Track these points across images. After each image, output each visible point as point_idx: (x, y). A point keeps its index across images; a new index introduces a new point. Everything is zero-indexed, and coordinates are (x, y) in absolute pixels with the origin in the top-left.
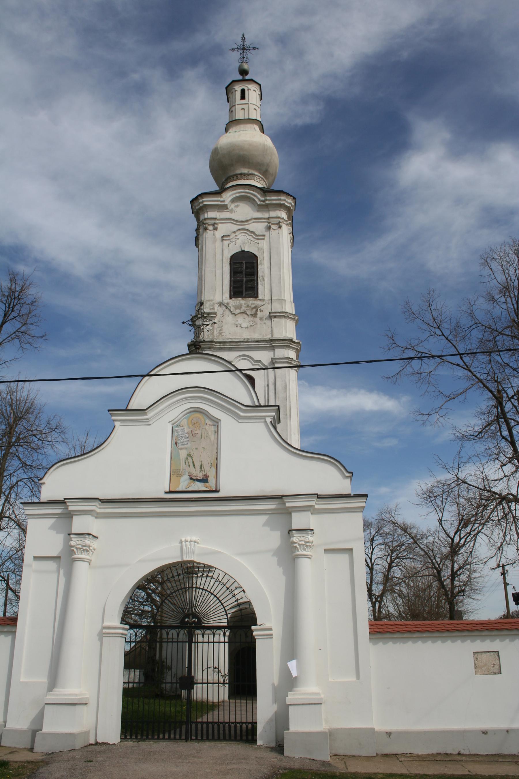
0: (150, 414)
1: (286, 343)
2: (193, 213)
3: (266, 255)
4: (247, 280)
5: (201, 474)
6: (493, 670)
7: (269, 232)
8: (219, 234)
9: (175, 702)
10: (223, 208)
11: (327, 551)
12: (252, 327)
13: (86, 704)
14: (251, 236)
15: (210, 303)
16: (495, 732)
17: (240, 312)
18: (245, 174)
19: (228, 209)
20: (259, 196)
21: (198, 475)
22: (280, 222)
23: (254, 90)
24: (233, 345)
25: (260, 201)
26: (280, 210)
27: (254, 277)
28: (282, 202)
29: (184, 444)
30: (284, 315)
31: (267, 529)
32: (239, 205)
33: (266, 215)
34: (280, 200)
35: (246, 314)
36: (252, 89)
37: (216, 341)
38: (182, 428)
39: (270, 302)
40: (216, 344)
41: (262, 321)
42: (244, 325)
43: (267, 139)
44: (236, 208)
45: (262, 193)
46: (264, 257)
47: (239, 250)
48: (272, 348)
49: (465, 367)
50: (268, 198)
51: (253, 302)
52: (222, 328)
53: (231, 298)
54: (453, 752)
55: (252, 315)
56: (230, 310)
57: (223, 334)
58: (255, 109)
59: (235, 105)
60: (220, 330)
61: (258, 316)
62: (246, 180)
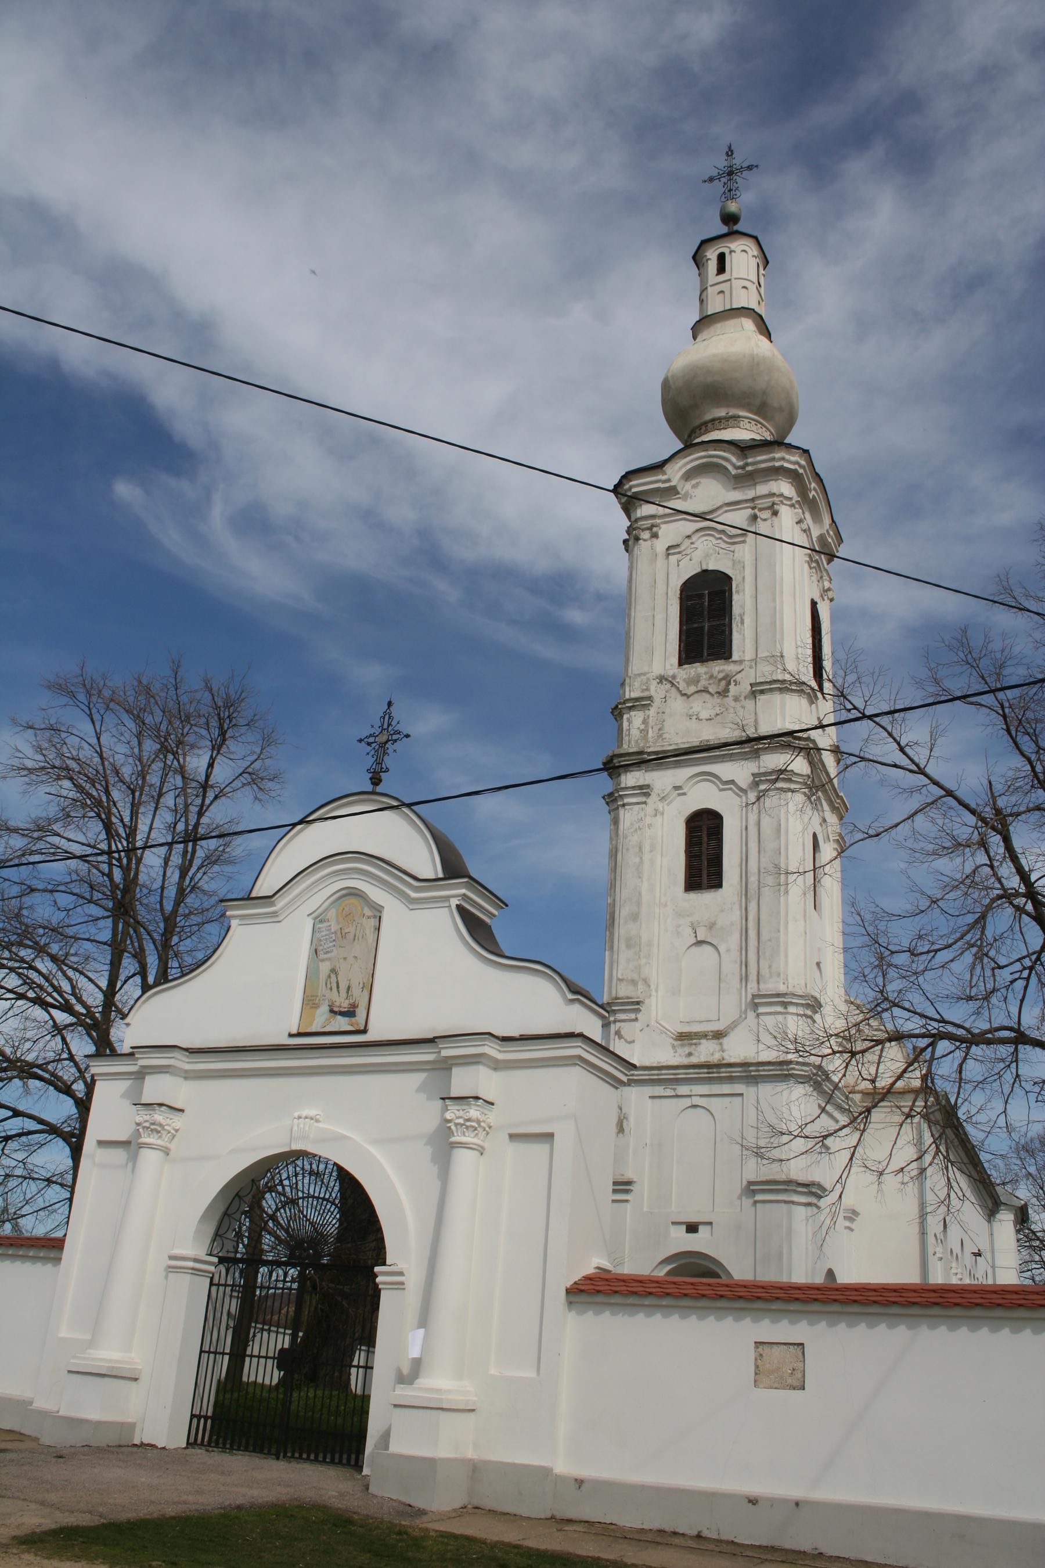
0: (280, 903)
3: (749, 573)
4: (710, 628)
5: (347, 1002)
6: (789, 1381)
8: (661, 545)
11: (512, 1136)
13: (136, 1379)
14: (720, 538)
16: (774, 1502)
17: (696, 690)
18: (720, 419)
19: (678, 493)
20: (734, 459)
21: (343, 1005)
22: (774, 504)
25: (737, 468)
26: (776, 480)
28: (777, 464)
29: (328, 952)
30: (779, 686)
31: (423, 1096)
32: (700, 482)
33: (750, 494)
34: (773, 459)
35: (708, 692)
36: (738, 249)
37: (649, 750)
38: (329, 924)
39: (753, 664)
42: (704, 715)
43: (759, 343)
44: (693, 490)
45: (739, 452)
46: (744, 578)
47: (699, 570)
48: (756, 754)
49: (914, 768)
50: (750, 460)
51: (722, 668)
53: (680, 664)
54: (688, 1532)
55: (718, 693)
56: (678, 689)
57: (665, 736)
58: (744, 287)
59: (706, 288)
60: (660, 729)
62: (722, 431)
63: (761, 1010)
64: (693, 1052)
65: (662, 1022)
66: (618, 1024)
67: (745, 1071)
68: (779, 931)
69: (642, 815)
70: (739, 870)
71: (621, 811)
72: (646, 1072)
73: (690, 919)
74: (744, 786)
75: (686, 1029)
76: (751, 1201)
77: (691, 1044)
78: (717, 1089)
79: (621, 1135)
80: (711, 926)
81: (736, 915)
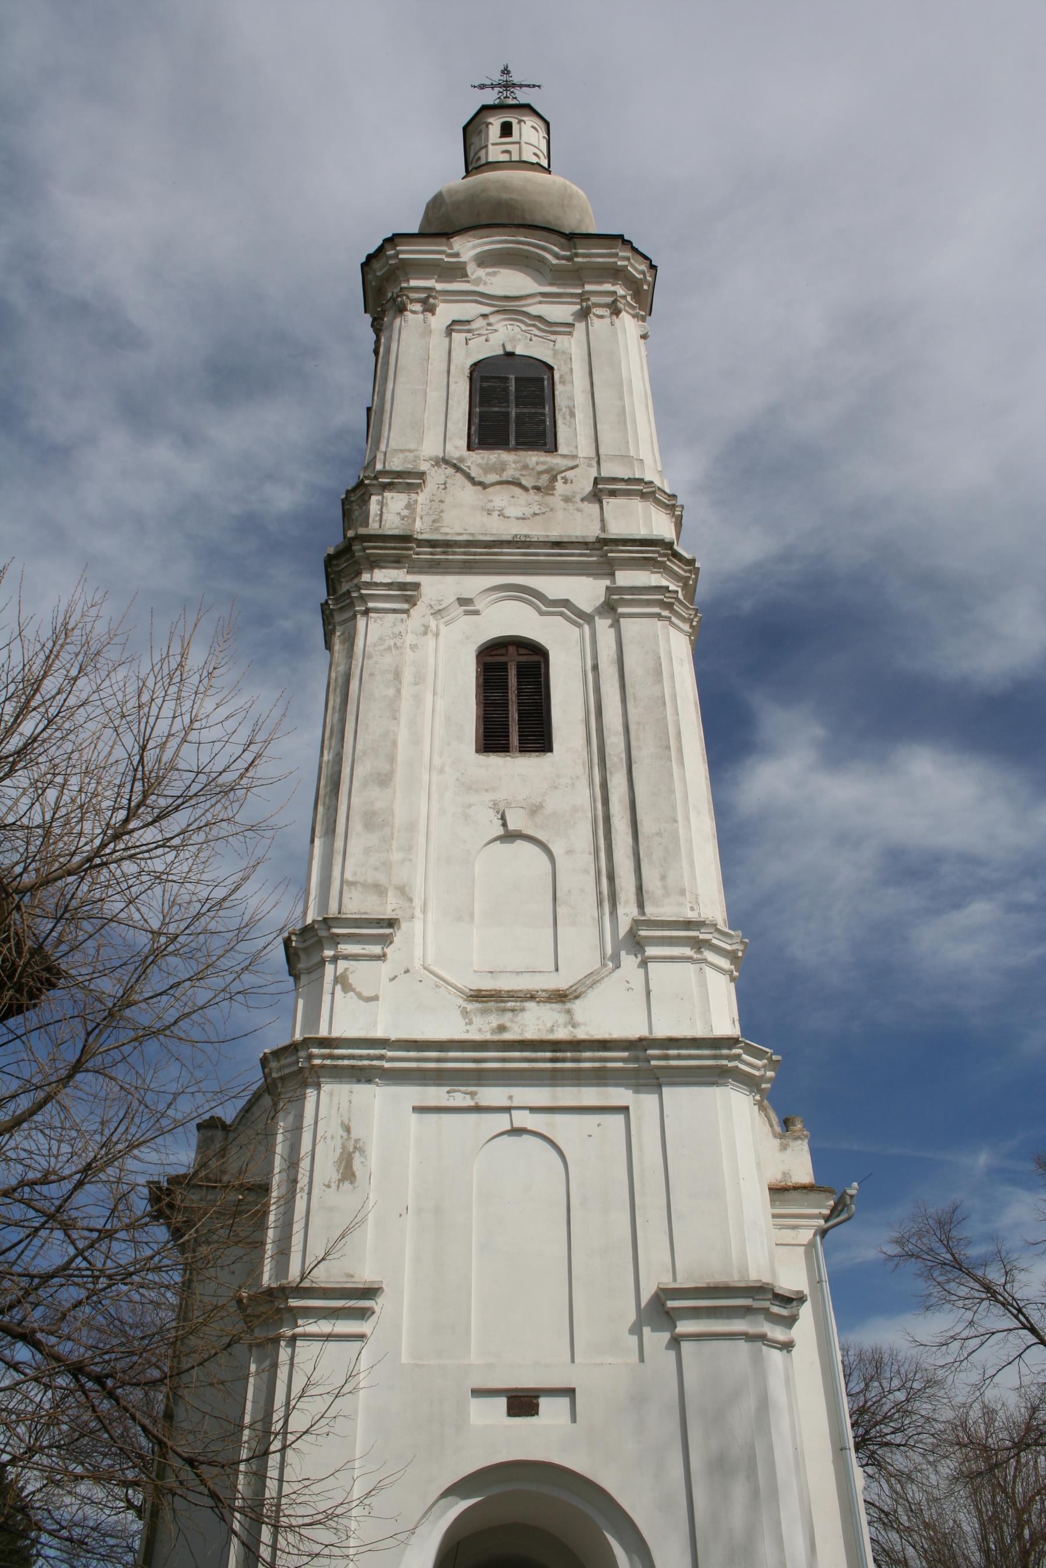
1: (654, 552)
2: (366, 312)
4: (518, 415)
7: (584, 323)
10: (457, 271)
12: (537, 517)
14: (534, 326)
15: (406, 457)
19: (467, 276)
23: (533, 127)
24: (475, 554)
27: (544, 408)
37: (420, 537)
42: (512, 511)
46: (572, 369)
51: (542, 459)
60: (434, 521)
61: (556, 493)
63: (651, 951)
64: (508, 1024)
65: (432, 967)
66: (342, 964)
67: (636, 1060)
68: (676, 821)
69: (401, 628)
71: (361, 622)
73: (488, 797)
74: (588, 609)
75: (488, 984)
76: (666, 1336)
77: (504, 1010)
79: (347, 1185)
80: (535, 810)
81: (582, 797)
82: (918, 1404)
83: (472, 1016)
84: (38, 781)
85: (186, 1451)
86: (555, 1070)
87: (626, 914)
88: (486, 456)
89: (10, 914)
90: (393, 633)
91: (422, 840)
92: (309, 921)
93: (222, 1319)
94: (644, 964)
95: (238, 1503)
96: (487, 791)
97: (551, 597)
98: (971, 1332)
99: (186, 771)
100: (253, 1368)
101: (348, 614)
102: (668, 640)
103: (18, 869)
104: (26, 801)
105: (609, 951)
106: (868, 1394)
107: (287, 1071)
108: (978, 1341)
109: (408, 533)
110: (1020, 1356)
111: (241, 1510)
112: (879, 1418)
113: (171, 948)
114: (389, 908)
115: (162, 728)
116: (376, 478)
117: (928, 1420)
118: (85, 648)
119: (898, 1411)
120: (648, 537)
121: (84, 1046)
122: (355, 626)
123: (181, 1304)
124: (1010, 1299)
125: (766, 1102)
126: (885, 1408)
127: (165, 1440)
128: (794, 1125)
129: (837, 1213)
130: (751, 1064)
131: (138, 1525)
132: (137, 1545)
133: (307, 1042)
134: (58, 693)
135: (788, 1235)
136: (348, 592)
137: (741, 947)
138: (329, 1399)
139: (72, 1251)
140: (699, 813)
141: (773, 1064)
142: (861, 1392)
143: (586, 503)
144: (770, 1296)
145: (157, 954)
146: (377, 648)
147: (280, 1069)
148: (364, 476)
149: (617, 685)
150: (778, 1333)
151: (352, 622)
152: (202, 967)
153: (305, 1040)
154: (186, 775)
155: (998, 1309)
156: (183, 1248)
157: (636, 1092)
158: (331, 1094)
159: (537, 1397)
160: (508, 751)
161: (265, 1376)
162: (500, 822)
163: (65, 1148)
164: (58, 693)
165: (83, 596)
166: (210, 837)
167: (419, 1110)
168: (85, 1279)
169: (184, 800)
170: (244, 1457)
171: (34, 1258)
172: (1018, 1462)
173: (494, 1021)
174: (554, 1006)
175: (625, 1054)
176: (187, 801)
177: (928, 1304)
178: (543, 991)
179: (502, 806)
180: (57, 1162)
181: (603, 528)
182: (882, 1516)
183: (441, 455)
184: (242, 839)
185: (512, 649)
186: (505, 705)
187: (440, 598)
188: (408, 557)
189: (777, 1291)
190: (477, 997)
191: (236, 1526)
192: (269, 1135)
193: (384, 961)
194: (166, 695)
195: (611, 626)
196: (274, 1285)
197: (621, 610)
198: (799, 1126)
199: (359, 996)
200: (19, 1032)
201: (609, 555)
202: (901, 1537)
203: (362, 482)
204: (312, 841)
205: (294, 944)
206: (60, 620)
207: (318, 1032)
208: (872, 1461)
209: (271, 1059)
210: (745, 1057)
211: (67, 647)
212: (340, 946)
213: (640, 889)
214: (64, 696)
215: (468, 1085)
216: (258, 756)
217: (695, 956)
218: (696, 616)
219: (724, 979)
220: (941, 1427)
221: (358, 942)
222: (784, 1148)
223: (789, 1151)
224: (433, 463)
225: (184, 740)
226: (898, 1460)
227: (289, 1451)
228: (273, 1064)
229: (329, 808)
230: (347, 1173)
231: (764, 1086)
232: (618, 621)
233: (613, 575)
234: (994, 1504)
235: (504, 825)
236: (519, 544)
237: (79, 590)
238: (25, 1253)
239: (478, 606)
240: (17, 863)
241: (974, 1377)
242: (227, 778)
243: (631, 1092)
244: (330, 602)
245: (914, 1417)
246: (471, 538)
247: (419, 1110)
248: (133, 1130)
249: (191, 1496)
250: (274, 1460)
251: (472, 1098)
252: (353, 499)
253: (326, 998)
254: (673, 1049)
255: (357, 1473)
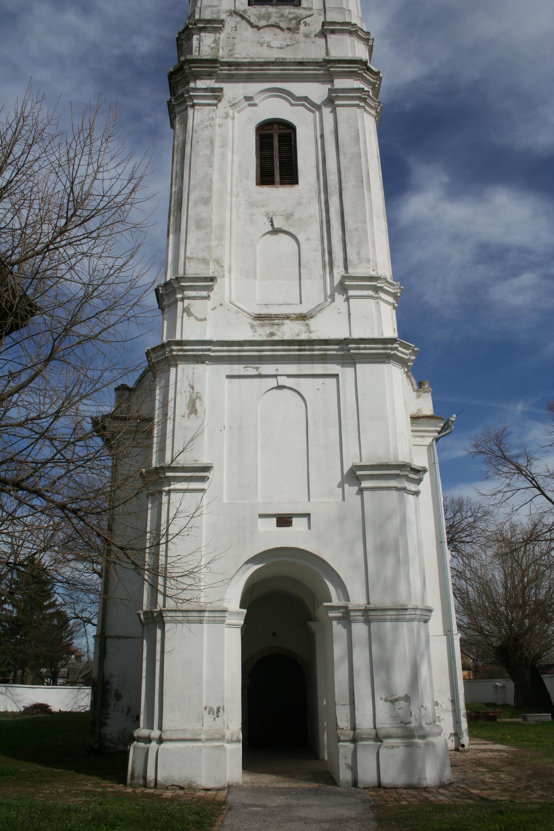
1: (356, 67)
9: (59, 589)
12: (289, 47)
15: (213, 10)
24: (254, 70)
37: (222, 60)
40: (221, 66)
41: (308, 39)
42: (275, 44)
51: (292, 10)
52: (234, 47)
60: (230, 50)
63: (351, 293)
64: (275, 332)
66: (187, 302)
67: (343, 350)
68: (365, 222)
69: (213, 115)
70: (315, 171)
71: (190, 111)
72: (225, 348)
73: (263, 210)
74: (318, 102)
76: (356, 488)
77: (273, 324)
78: (307, 369)
79: (193, 416)
80: (288, 217)
82: (479, 523)
83: (256, 328)
84: (15, 204)
85: (119, 544)
86: (300, 355)
87: (338, 273)
88: (259, 9)
89: (7, 276)
90: (209, 118)
91: (228, 234)
92: (168, 279)
93: (133, 482)
94: (347, 299)
95: (147, 567)
96: (262, 206)
97: (297, 95)
98: (509, 489)
99: (97, 195)
100: (150, 506)
101: (183, 107)
102: (363, 120)
103: (9, 253)
104: (10, 215)
105: (329, 293)
106: (455, 519)
107: (159, 359)
108: (511, 493)
109: (215, 58)
110: (531, 500)
111: (148, 570)
112: (459, 530)
113: (95, 294)
114: (211, 271)
115: (82, 171)
116: (195, 24)
117: (483, 530)
118: (35, 127)
119: (469, 527)
120: (353, 59)
121: (53, 346)
122: (187, 114)
123: (112, 475)
124: (529, 473)
125: (410, 373)
126: (463, 525)
127: (109, 539)
128: (424, 385)
129: (444, 430)
130: (403, 352)
131: (100, 581)
132: (100, 589)
133: (170, 343)
134: (23, 154)
135: (419, 441)
136: (183, 94)
137: (399, 291)
138: (188, 519)
139: (55, 451)
140: (378, 218)
141: (414, 353)
142: (452, 518)
143: (317, 38)
144: (409, 469)
145: (87, 297)
146: (200, 127)
147: (156, 357)
148: (189, 23)
149: (334, 146)
150: (412, 487)
151: (185, 112)
152: (112, 303)
153: (169, 342)
154: (97, 197)
155: (522, 478)
156: (111, 448)
157: (343, 366)
158: (183, 370)
159: (292, 518)
160: (274, 184)
161: (156, 509)
162: (270, 223)
163: (48, 400)
164: (23, 154)
165: (31, 96)
166: (113, 232)
167: (229, 377)
168: (63, 464)
169: (97, 211)
170: (148, 546)
171: (37, 455)
172: (525, 549)
173: (268, 330)
174: (299, 322)
175: (337, 347)
176: (98, 212)
177: (487, 475)
178: (294, 314)
179: (271, 215)
180: (44, 408)
181: (327, 54)
182: (458, 574)
183: (233, 9)
184: (130, 232)
185: (275, 126)
186: (272, 158)
187: (235, 97)
188: (217, 72)
189: (412, 467)
190: (259, 317)
191: (146, 577)
192: (153, 391)
193: (209, 300)
194: (83, 152)
195: (331, 112)
196: (158, 466)
197: (337, 102)
198: (427, 386)
199: (196, 318)
200: (18, 341)
201: (331, 69)
202: (466, 583)
203: (188, 26)
204: (168, 236)
205: (160, 292)
206: (19, 111)
207: (175, 338)
208: (455, 549)
209: (151, 352)
210: (400, 349)
211: (25, 127)
212: (185, 292)
213: (345, 259)
214: (26, 155)
215: (254, 364)
216: (136, 186)
217: (375, 295)
218: (379, 106)
219: (390, 308)
220: (490, 534)
221: (195, 290)
222: (418, 397)
223: (421, 398)
224: (229, 14)
225: (95, 178)
226: (468, 549)
227: (169, 543)
228: (153, 356)
229: (177, 217)
230: (193, 410)
231: (409, 364)
232: (335, 109)
233: (332, 81)
234: (512, 567)
235: (272, 225)
236: (279, 64)
237: (28, 92)
238: (32, 452)
239: (256, 101)
240: (8, 251)
241: (508, 510)
242: (119, 199)
243: (340, 366)
244: (172, 100)
245: (477, 530)
246: (251, 60)
247: (229, 377)
248: (81, 391)
249: (123, 564)
250: (162, 547)
251: (257, 371)
252: (182, 37)
253: (179, 320)
254: (362, 344)
255: (203, 553)
